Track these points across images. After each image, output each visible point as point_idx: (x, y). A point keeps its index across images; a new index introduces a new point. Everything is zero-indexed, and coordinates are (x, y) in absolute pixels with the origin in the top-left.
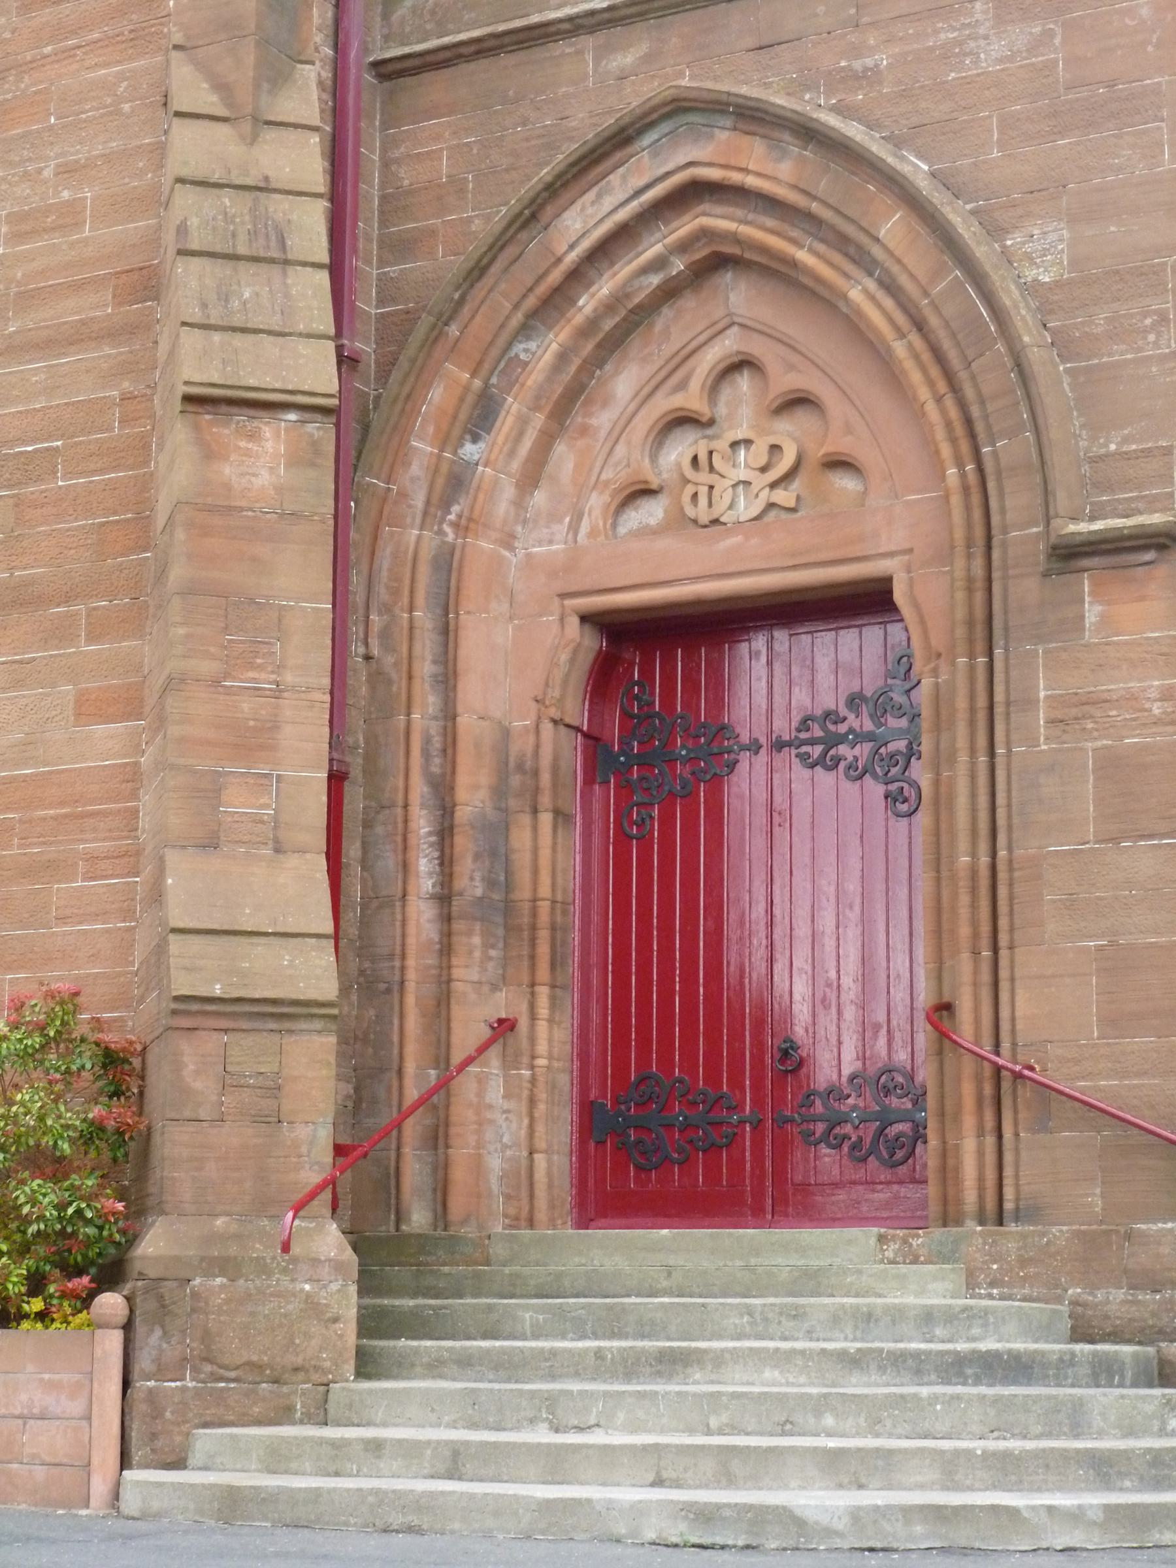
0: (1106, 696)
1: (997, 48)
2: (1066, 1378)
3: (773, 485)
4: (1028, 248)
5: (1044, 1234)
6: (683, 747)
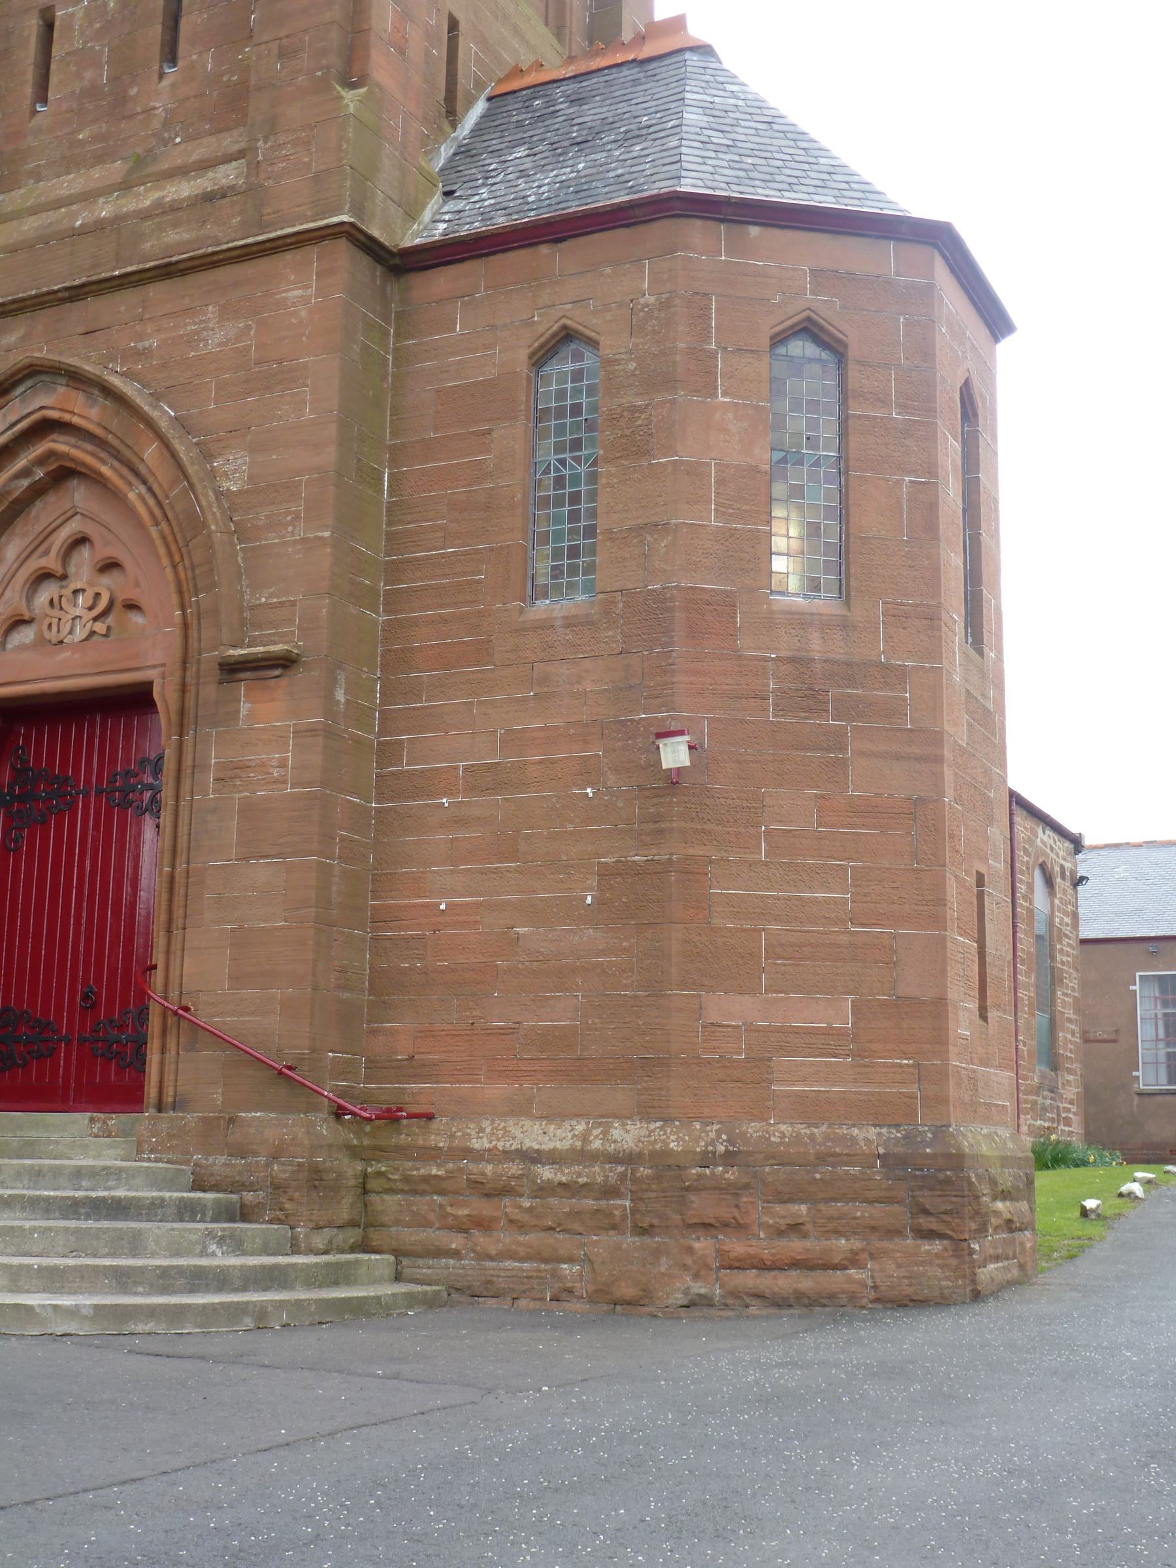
0: (248, 763)
1: (219, 336)
2: (156, 1215)
3: (95, 619)
4: (226, 468)
5: (183, 1118)
6: (44, 791)
